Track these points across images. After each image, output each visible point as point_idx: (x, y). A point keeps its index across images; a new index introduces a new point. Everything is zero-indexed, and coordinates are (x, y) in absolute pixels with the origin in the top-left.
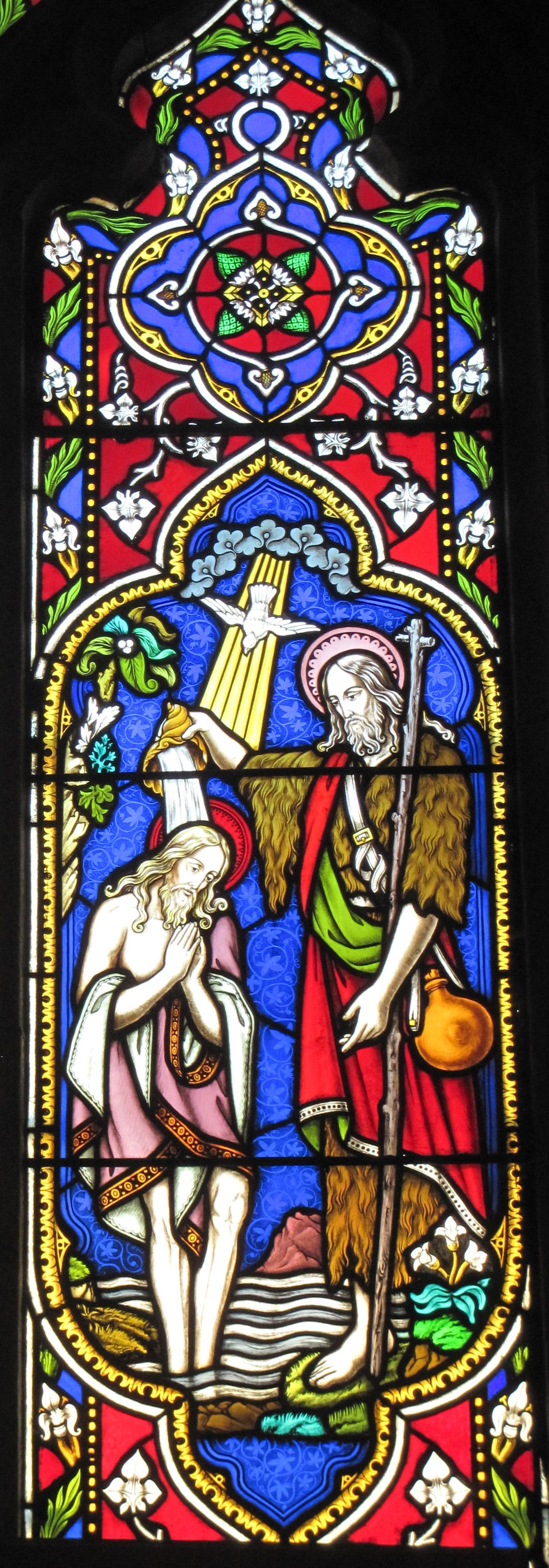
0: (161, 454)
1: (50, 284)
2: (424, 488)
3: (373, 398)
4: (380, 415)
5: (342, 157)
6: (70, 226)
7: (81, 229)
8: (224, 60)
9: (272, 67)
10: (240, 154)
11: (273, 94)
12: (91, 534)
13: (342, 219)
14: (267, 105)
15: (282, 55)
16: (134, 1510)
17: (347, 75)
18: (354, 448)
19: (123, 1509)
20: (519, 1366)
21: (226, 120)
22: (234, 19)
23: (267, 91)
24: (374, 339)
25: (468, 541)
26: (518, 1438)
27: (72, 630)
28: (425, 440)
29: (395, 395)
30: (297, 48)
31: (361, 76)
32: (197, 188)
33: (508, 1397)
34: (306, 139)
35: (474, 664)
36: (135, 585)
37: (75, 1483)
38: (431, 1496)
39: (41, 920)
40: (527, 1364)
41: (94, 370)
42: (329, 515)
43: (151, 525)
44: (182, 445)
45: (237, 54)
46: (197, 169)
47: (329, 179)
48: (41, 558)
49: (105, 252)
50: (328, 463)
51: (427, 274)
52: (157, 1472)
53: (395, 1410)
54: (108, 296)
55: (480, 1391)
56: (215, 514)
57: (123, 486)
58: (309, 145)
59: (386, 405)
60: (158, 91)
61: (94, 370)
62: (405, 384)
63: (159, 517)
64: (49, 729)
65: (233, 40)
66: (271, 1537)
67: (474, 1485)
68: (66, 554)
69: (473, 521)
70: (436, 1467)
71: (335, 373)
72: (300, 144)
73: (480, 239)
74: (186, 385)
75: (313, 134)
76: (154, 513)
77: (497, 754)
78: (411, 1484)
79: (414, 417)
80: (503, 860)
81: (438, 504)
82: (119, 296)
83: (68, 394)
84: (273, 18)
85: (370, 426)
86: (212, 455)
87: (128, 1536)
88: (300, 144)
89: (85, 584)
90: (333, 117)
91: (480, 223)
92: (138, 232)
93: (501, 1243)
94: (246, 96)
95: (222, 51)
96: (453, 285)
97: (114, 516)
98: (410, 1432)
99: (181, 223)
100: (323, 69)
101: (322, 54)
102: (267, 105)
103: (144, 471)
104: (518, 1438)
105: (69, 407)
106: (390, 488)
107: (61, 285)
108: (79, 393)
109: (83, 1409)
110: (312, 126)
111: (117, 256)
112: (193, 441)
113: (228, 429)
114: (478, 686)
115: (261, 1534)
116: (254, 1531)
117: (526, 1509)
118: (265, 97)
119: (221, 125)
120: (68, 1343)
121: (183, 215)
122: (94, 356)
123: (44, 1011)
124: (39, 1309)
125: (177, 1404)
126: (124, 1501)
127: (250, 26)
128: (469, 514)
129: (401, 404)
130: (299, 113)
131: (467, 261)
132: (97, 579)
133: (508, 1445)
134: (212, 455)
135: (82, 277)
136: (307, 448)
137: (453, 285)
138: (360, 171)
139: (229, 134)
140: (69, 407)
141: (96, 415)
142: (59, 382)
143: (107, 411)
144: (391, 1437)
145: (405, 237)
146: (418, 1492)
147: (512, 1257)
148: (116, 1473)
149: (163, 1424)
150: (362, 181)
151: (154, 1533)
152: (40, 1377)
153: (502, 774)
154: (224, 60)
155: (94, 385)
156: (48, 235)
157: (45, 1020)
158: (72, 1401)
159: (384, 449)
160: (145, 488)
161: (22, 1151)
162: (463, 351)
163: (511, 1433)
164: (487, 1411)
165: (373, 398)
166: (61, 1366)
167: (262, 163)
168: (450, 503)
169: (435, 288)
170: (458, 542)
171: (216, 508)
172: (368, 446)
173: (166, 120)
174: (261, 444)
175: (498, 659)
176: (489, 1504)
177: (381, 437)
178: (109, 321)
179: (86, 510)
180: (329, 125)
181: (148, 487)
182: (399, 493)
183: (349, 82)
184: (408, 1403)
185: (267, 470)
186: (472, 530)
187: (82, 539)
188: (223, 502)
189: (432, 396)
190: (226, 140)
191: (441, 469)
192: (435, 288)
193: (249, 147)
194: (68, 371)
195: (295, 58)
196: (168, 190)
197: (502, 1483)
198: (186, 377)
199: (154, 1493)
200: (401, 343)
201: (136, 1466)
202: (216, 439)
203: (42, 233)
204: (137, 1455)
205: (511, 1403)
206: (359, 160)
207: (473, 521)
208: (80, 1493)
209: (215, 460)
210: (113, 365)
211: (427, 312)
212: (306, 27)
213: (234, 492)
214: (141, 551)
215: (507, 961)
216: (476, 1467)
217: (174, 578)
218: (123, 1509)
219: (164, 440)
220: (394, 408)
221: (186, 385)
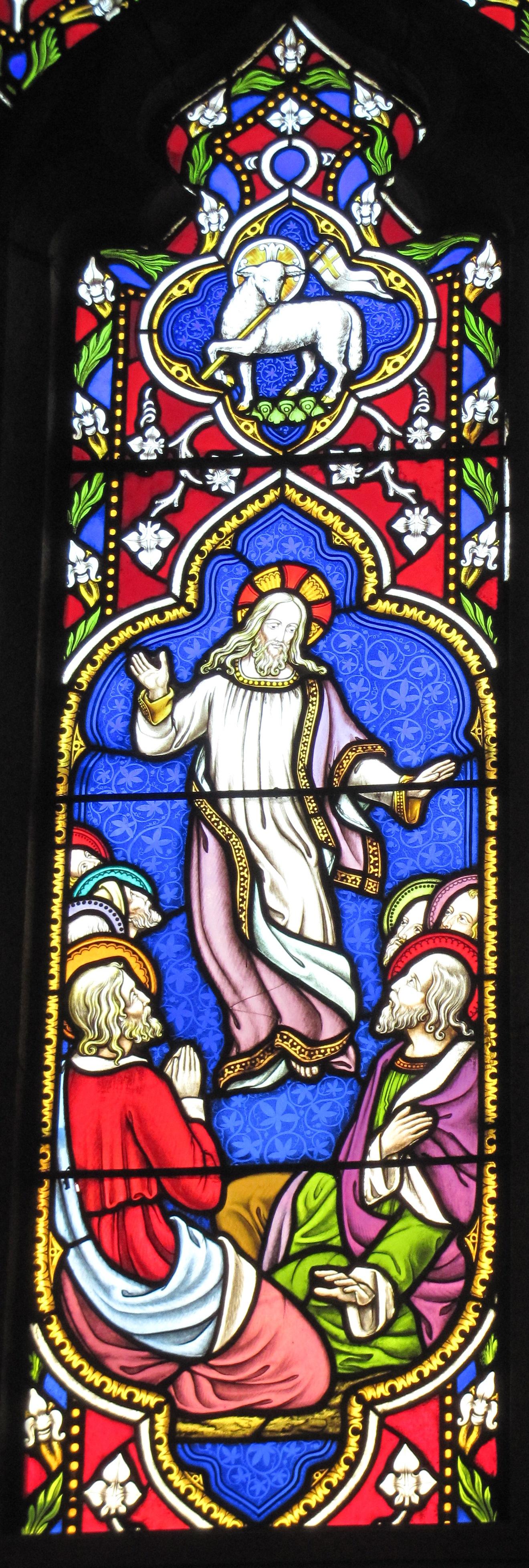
0: (181, 485)
1: (84, 323)
3: (386, 426)
4: (393, 443)
5: (369, 194)
6: (103, 266)
7: (114, 268)
8: (257, 100)
9: (303, 105)
10: (269, 192)
11: (304, 133)
13: (365, 254)
14: (297, 143)
15: (313, 94)
17: (376, 112)
20: (489, 1358)
21: (256, 158)
22: (267, 62)
23: (298, 128)
24: (391, 371)
25: (472, 564)
26: (483, 1425)
28: (437, 465)
29: (410, 420)
30: (328, 88)
31: (388, 113)
32: (229, 225)
34: (333, 176)
35: (472, 681)
36: (150, 614)
38: (402, 1476)
40: (498, 1354)
41: (123, 405)
42: (338, 543)
43: (170, 554)
44: (201, 476)
45: (272, 94)
46: (228, 207)
47: (356, 215)
49: (138, 290)
51: (444, 306)
52: (139, 1475)
53: (368, 1406)
54: (138, 331)
55: (453, 1379)
57: (145, 517)
58: (335, 183)
59: (400, 434)
60: (194, 132)
61: (123, 405)
62: (419, 414)
65: (266, 82)
69: (478, 543)
70: (406, 1459)
71: (353, 404)
72: (327, 181)
73: (497, 274)
74: (209, 418)
75: (339, 172)
77: (492, 769)
78: (381, 1479)
79: (428, 446)
80: (494, 923)
82: (150, 331)
83: (97, 431)
84: (305, 58)
85: (382, 456)
86: (231, 488)
88: (327, 181)
90: (360, 153)
91: (499, 258)
92: (168, 270)
93: (474, 1238)
94: (279, 135)
95: (254, 92)
96: (469, 317)
97: (134, 548)
98: (382, 1426)
99: (214, 259)
100: (352, 107)
101: (351, 94)
102: (297, 143)
103: (165, 503)
104: (483, 1425)
105: (97, 442)
106: (401, 514)
108: (107, 431)
110: (338, 165)
111: (149, 292)
112: (213, 475)
113: (248, 462)
114: (476, 703)
118: (296, 135)
119: (250, 163)
121: (214, 251)
122: (123, 391)
125: (159, 1408)
126: (103, 1504)
127: (284, 67)
128: (475, 537)
130: (327, 150)
131: (485, 294)
133: (476, 573)
134: (231, 488)
135: (64, 1467)
136: (320, 477)
138: (385, 208)
139: (258, 171)
140: (97, 442)
141: (125, 449)
143: (135, 444)
144: (362, 1434)
145: (423, 268)
146: (388, 1485)
149: (145, 1427)
150: (387, 215)
153: (494, 1166)
154: (257, 100)
155: (122, 420)
156: (82, 277)
158: (57, 1407)
159: (395, 477)
160: (165, 520)
162: (476, 380)
165: (386, 426)
167: (290, 199)
169: (452, 321)
173: (201, 162)
174: (277, 475)
175: (495, 235)
176: (454, 1498)
177: (394, 465)
178: (140, 358)
180: (357, 162)
181: (168, 518)
182: (408, 518)
183: (377, 120)
185: (283, 499)
189: (445, 425)
190: (255, 177)
192: (452, 321)
193: (277, 185)
195: (326, 97)
196: (199, 227)
198: (209, 409)
199: (134, 1494)
200: (416, 374)
201: (118, 1469)
202: (236, 472)
203: (75, 276)
204: (120, 1457)
206: (384, 196)
207: (478, 543)
209: (233, 492)
210: (141, 399)
211: (443, 343)
212: (336, 67)
214: (159, 579)
215: (494, 966)
217: (189, 606)
218: (104, 1512)
219: (184, 473)
220: (408, 436)
221: (209, 418)
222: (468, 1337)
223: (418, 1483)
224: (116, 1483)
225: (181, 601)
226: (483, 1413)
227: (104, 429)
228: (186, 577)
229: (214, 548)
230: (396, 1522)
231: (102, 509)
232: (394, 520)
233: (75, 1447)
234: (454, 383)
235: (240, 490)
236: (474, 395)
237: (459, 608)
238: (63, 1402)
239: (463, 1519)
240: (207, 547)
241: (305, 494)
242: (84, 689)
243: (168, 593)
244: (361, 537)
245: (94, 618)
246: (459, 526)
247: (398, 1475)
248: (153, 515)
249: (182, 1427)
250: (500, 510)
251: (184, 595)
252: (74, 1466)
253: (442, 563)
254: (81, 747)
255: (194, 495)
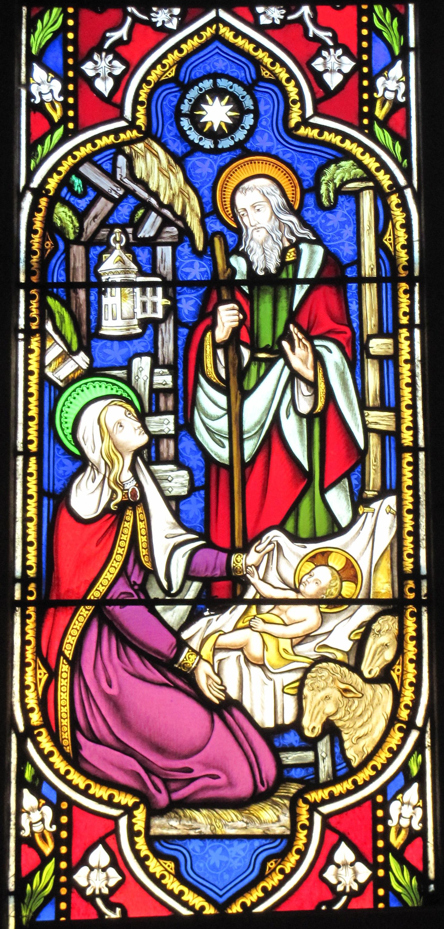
0: (129, 20)
2: (347, 52)
12: (71, 87)
16: (97, 892)
18: (290, 18)
19: (89, 892)
26: (410, 827)
27: (54, 170)
33: (388, 72)
37: (50, 868)
39: (26, 410)
48: (20, 840)
50: (270, 32)
55: (382, 790)
56: (173, 74)
57: (99, 49)
63: (127, 77)
64: (35, 253)
66: (210, 910)
67: (373, 866)
68: (43, 837)
76: (124, 73)
78: (324, 870)
81: (360, 64)
83: (44, 828)
86: (173, 25)
87: (94, 916)
89: (66, 130)
93: (390, 240)
96: (393, 863)
103: (115, 36)
104: (410, 827)
106: (318, 54)
107: (46, 126)
108: (62, 99)
109: (57, 813)
115: (203, 908)
116: (197, 907)
117: (416, 887)
120: (46, 758)
123: (30, 361)
124: (21, 728)
126: (89, 885)
129: (343, 882)
132: (76, 126)
133: (387, 105)
134: (173, 25)
135: (55, 853)
137: (393, 863)
142: (45, 89)
146: (330, 874)
147: (407, 682)
148: (84, 861)
151: (114, 911)
152: (21, 783)
157: (29, 515)
159: (314, 21)
161: (11, 445)
163: (405, 823)
164: (385, 806)
166: (38, 774)
168: (368, 63)
170: (375, 95)
171: (174, 69)
172: (302, 17)
174: (212, 15)
177: (313, 9)
179: (67, 68)
181: (120, 50)
184: (324, 802)
185: (217, 37)
186: (387, 86)
187: (64, 92)
188: (180, 63)
191: (361, 38)
194: (43, 805)
197: (398, 866)
202: (177, 11)
204: (100, 847)
205: (405, 800)
208: (53, 877)
213: (190, 55)
214: (115, 105)
216: (376, 851)
218: (89, 892)
222: (395, 753)
223: (355, 873)
224: (98, 868)
225: (129, 811)
226: (409, 817)
227: (51, 826)
228: (136, 102)
229: (159, 79)
230: (337, 907)
231: (53, 900)
232: (313, 59)
233: (64, 834)
234: (365, 19)
235: (181, 26)
236: (384, 76)
237: (372, 136)
238: (54, 800)
239: (394, 904)
240: (152, 78)
241: (238, 33)
242: (51, 194)
243: (121, 117)
244: (286, 72)
245: (59, 133)
246: (370, 58)
247: (338, 866)
248: (106, 46)
249: (153, 460)
250: (405, 49)
251: (135, 118)
252: (64, 850)
253: (370, 835)
254: (45, 674)
255: (139, 27)
